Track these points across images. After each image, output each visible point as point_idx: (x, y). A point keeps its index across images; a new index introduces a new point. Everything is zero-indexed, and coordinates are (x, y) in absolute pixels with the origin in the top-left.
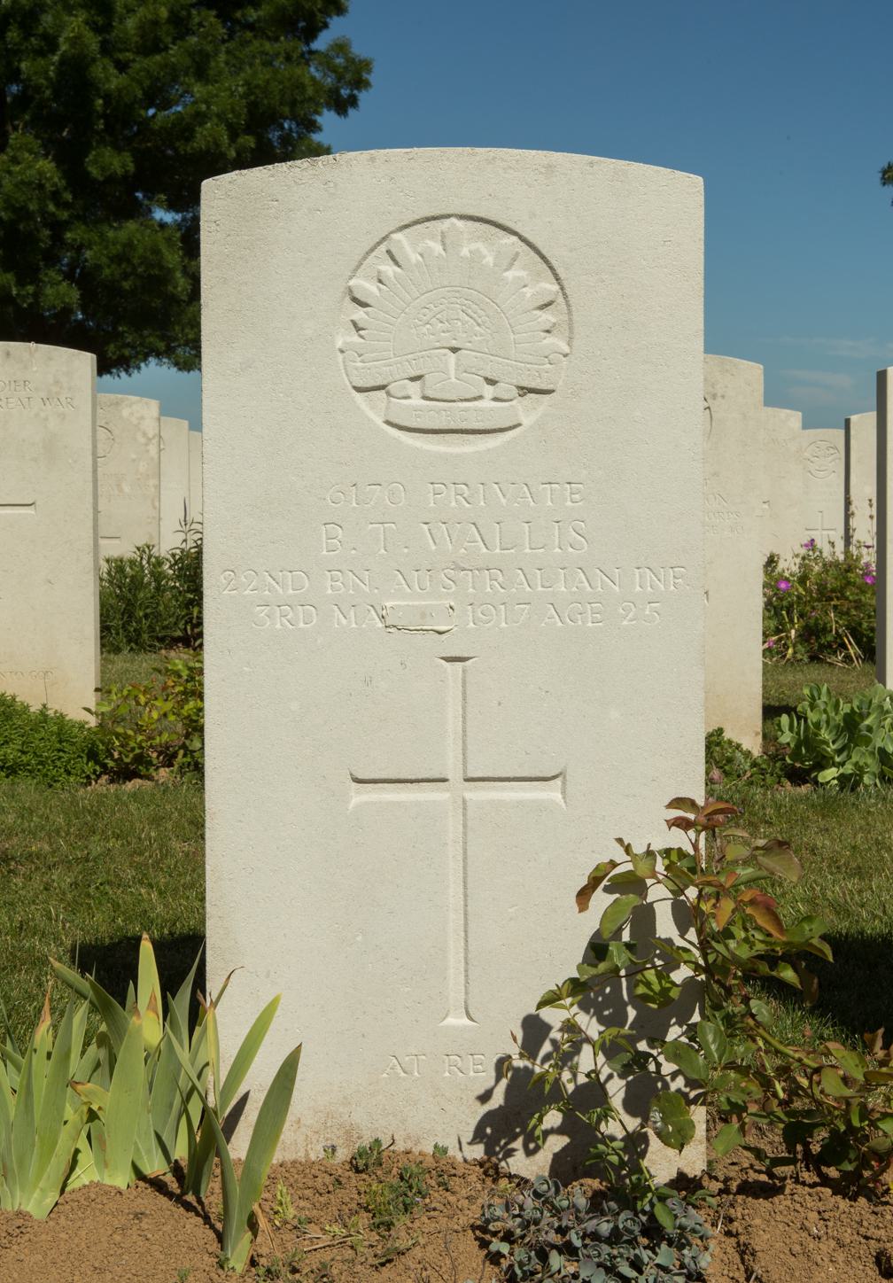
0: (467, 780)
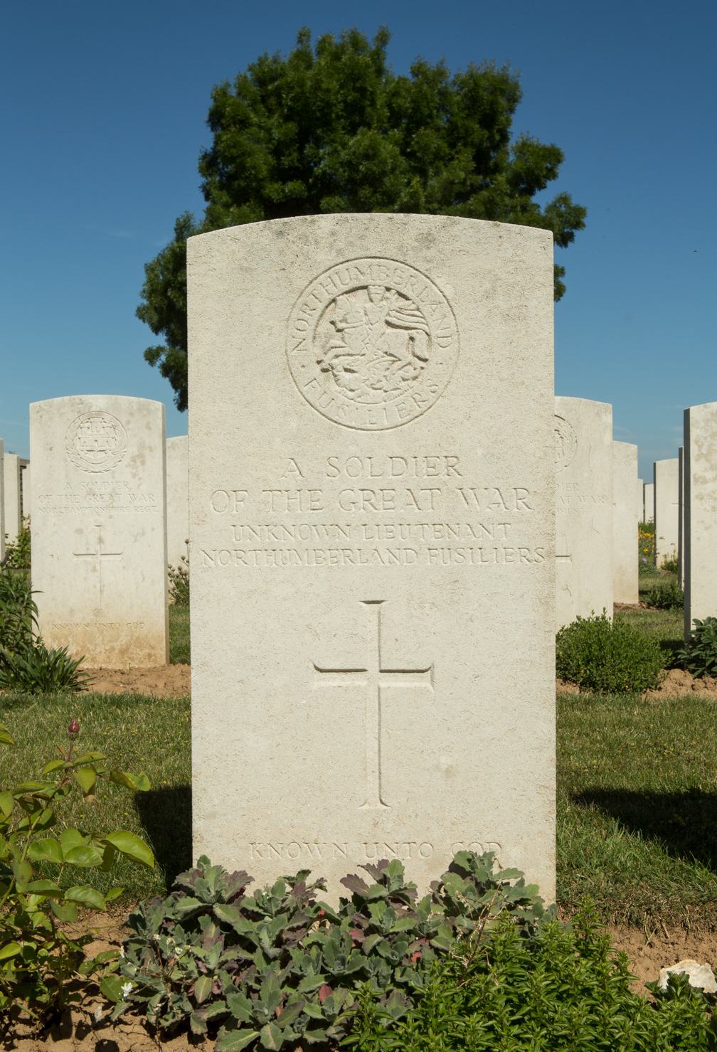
0: (382, 671)
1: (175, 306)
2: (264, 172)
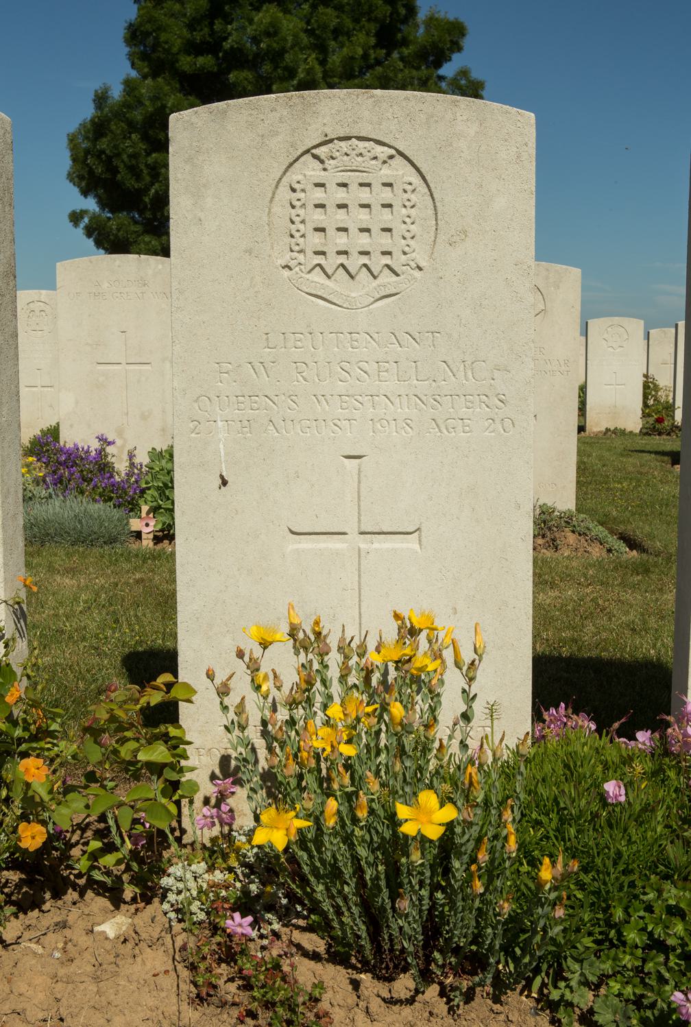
0: (362, 533)
1: (94, 172)
2: (177, 44)
